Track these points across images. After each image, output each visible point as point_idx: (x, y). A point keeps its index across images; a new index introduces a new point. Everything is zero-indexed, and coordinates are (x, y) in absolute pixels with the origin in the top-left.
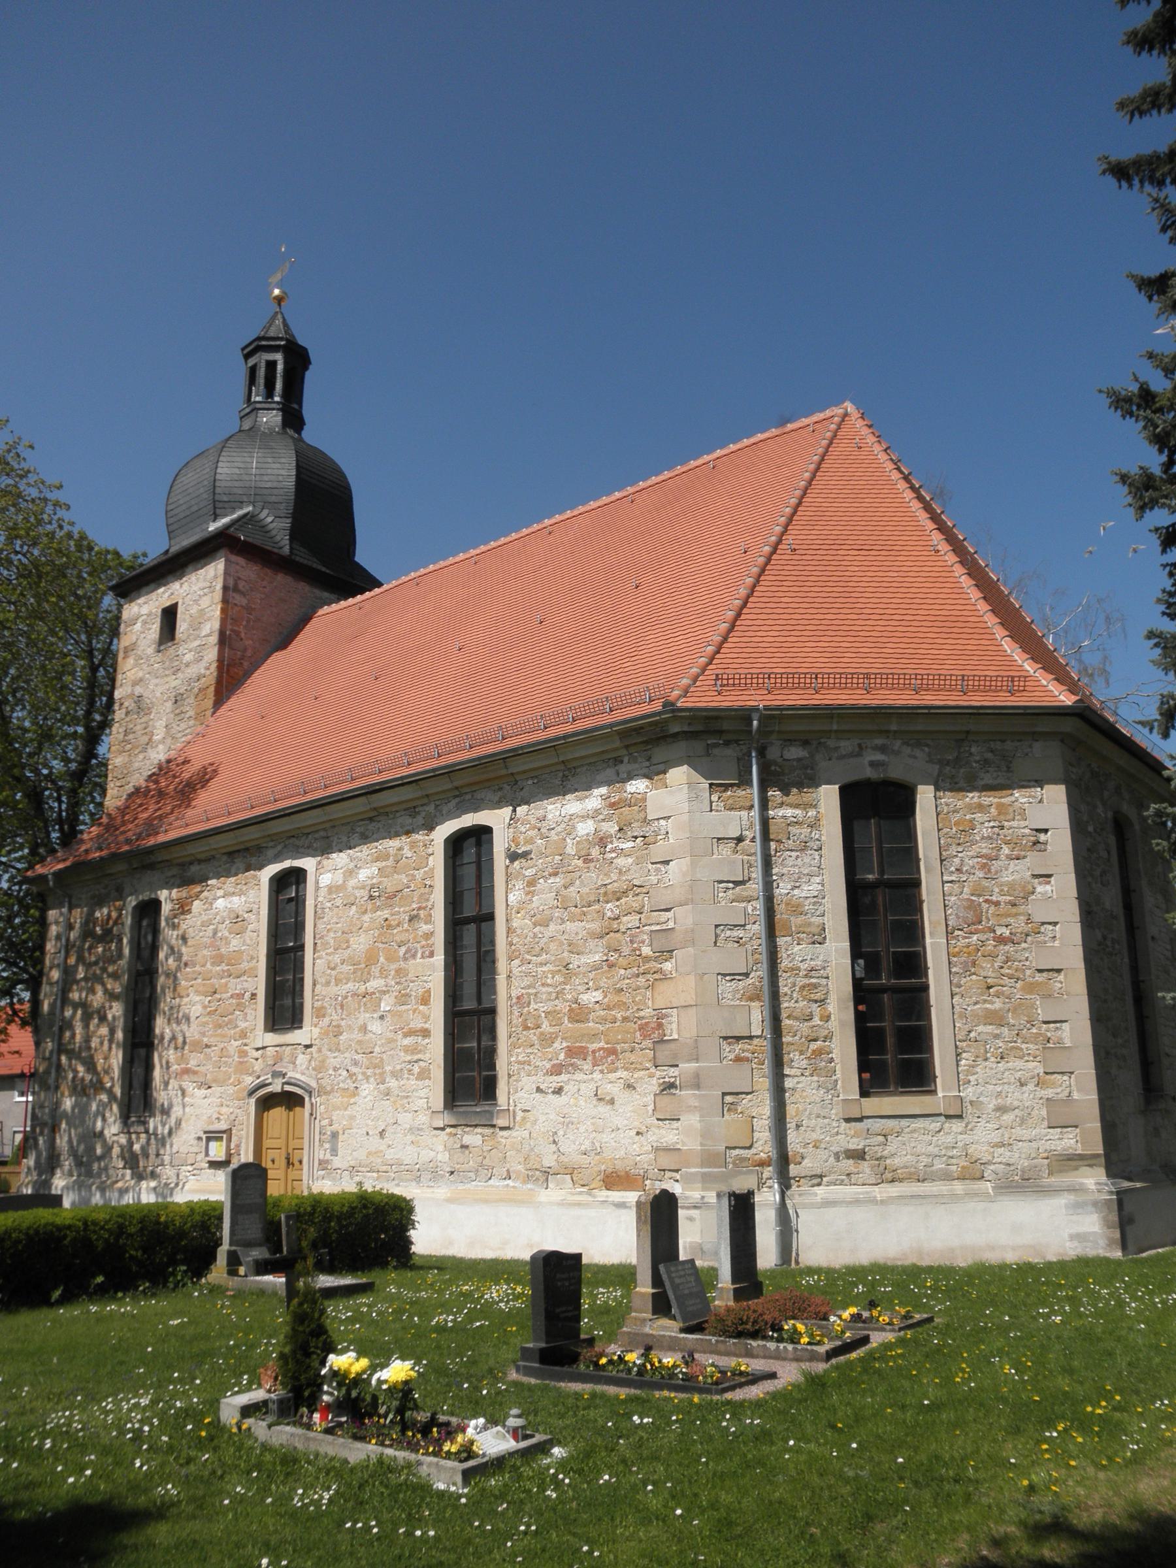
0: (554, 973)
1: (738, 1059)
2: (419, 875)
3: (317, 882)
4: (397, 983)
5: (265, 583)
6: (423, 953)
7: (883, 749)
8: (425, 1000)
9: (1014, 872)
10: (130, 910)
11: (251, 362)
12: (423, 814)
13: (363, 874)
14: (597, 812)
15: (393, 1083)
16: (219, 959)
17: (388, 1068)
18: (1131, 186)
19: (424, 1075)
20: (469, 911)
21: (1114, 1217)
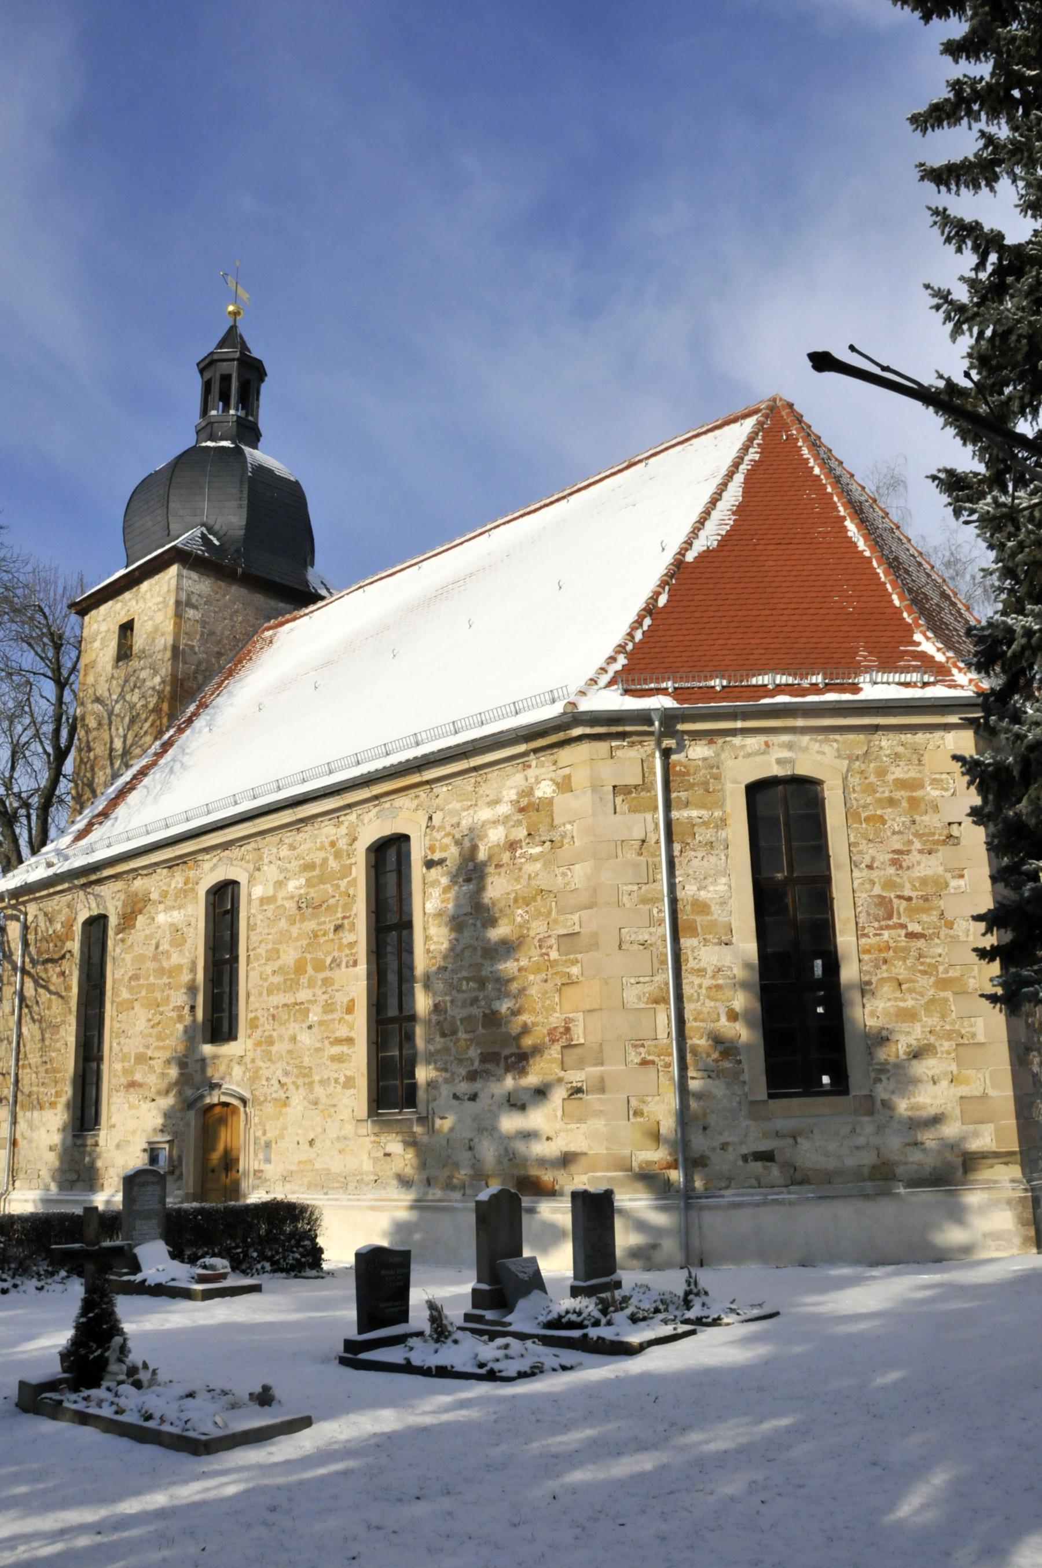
0: (468, 979)
1: (644, 1063)
2: (343, 883)
3: (250, 895)
4: (324, 993)
5: (218, 596)
6: (348, 962)
7: (790, 746)
8: (350, 1009)
9: (928, 867)
10: (80, 925)
11: (208, 375)
12: (346, 824)
13: (292, 886)
14: (507, 817)
15: (319, 1090)
16: (161, 971)
17: (317, 1078)
18: (949, 190)
19: (349, 1083)
20: (392, 919)
21: (1028, 1215)
